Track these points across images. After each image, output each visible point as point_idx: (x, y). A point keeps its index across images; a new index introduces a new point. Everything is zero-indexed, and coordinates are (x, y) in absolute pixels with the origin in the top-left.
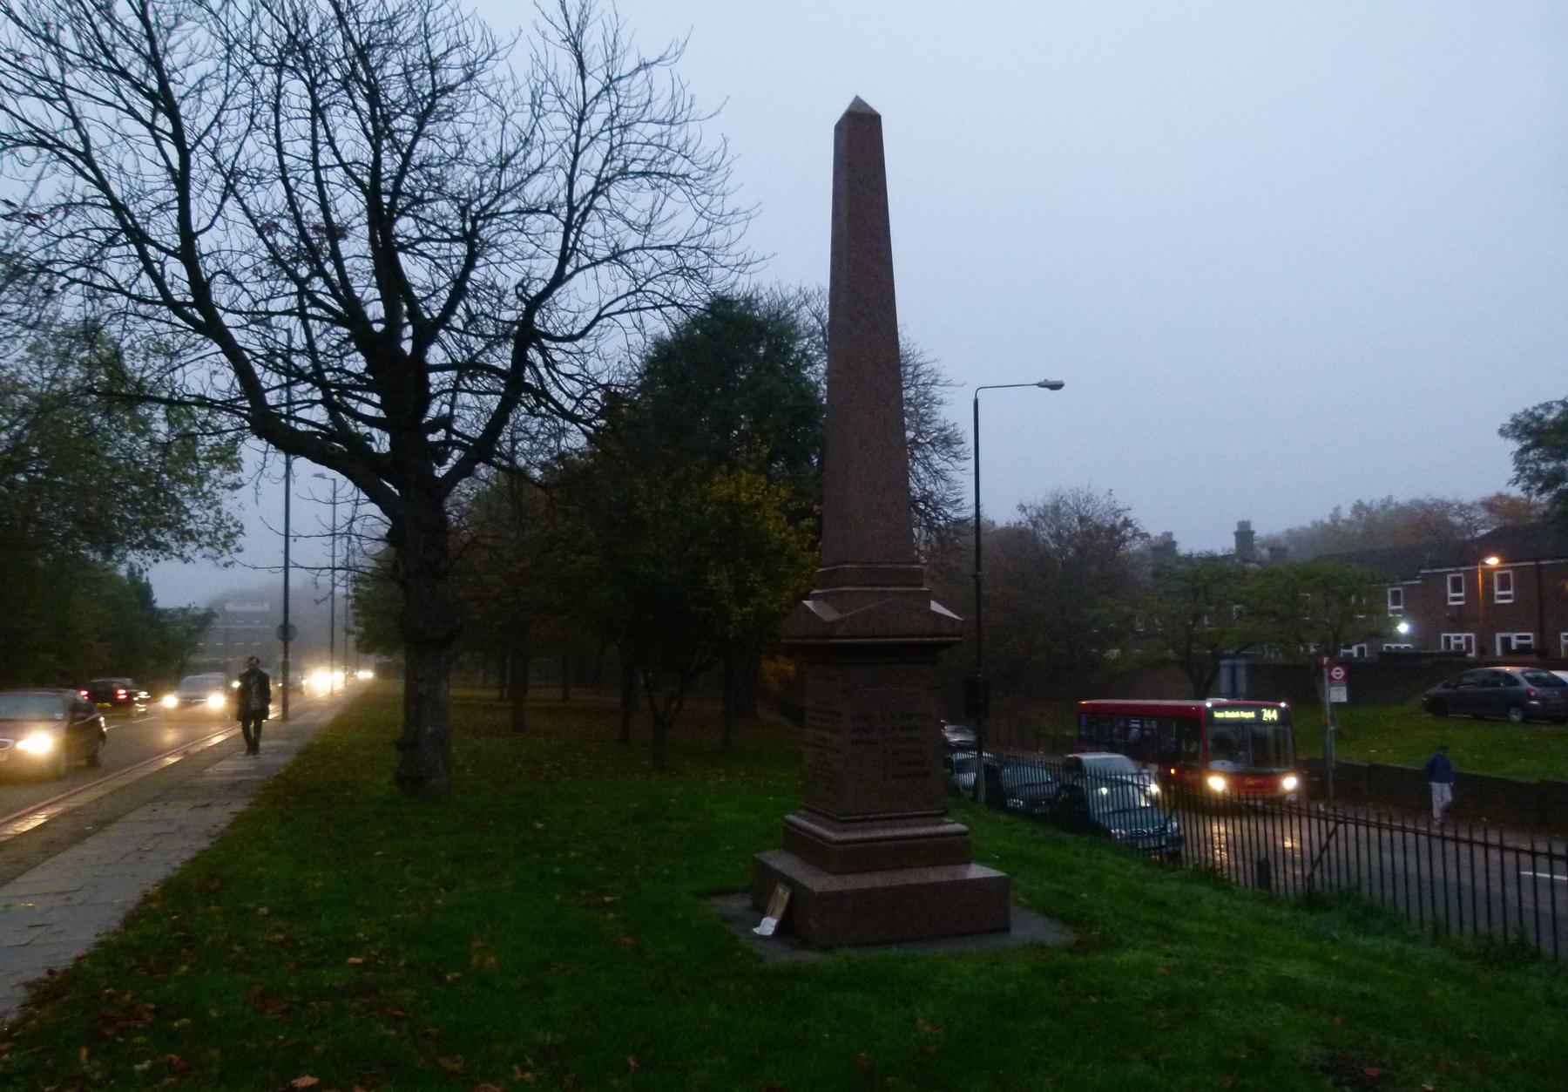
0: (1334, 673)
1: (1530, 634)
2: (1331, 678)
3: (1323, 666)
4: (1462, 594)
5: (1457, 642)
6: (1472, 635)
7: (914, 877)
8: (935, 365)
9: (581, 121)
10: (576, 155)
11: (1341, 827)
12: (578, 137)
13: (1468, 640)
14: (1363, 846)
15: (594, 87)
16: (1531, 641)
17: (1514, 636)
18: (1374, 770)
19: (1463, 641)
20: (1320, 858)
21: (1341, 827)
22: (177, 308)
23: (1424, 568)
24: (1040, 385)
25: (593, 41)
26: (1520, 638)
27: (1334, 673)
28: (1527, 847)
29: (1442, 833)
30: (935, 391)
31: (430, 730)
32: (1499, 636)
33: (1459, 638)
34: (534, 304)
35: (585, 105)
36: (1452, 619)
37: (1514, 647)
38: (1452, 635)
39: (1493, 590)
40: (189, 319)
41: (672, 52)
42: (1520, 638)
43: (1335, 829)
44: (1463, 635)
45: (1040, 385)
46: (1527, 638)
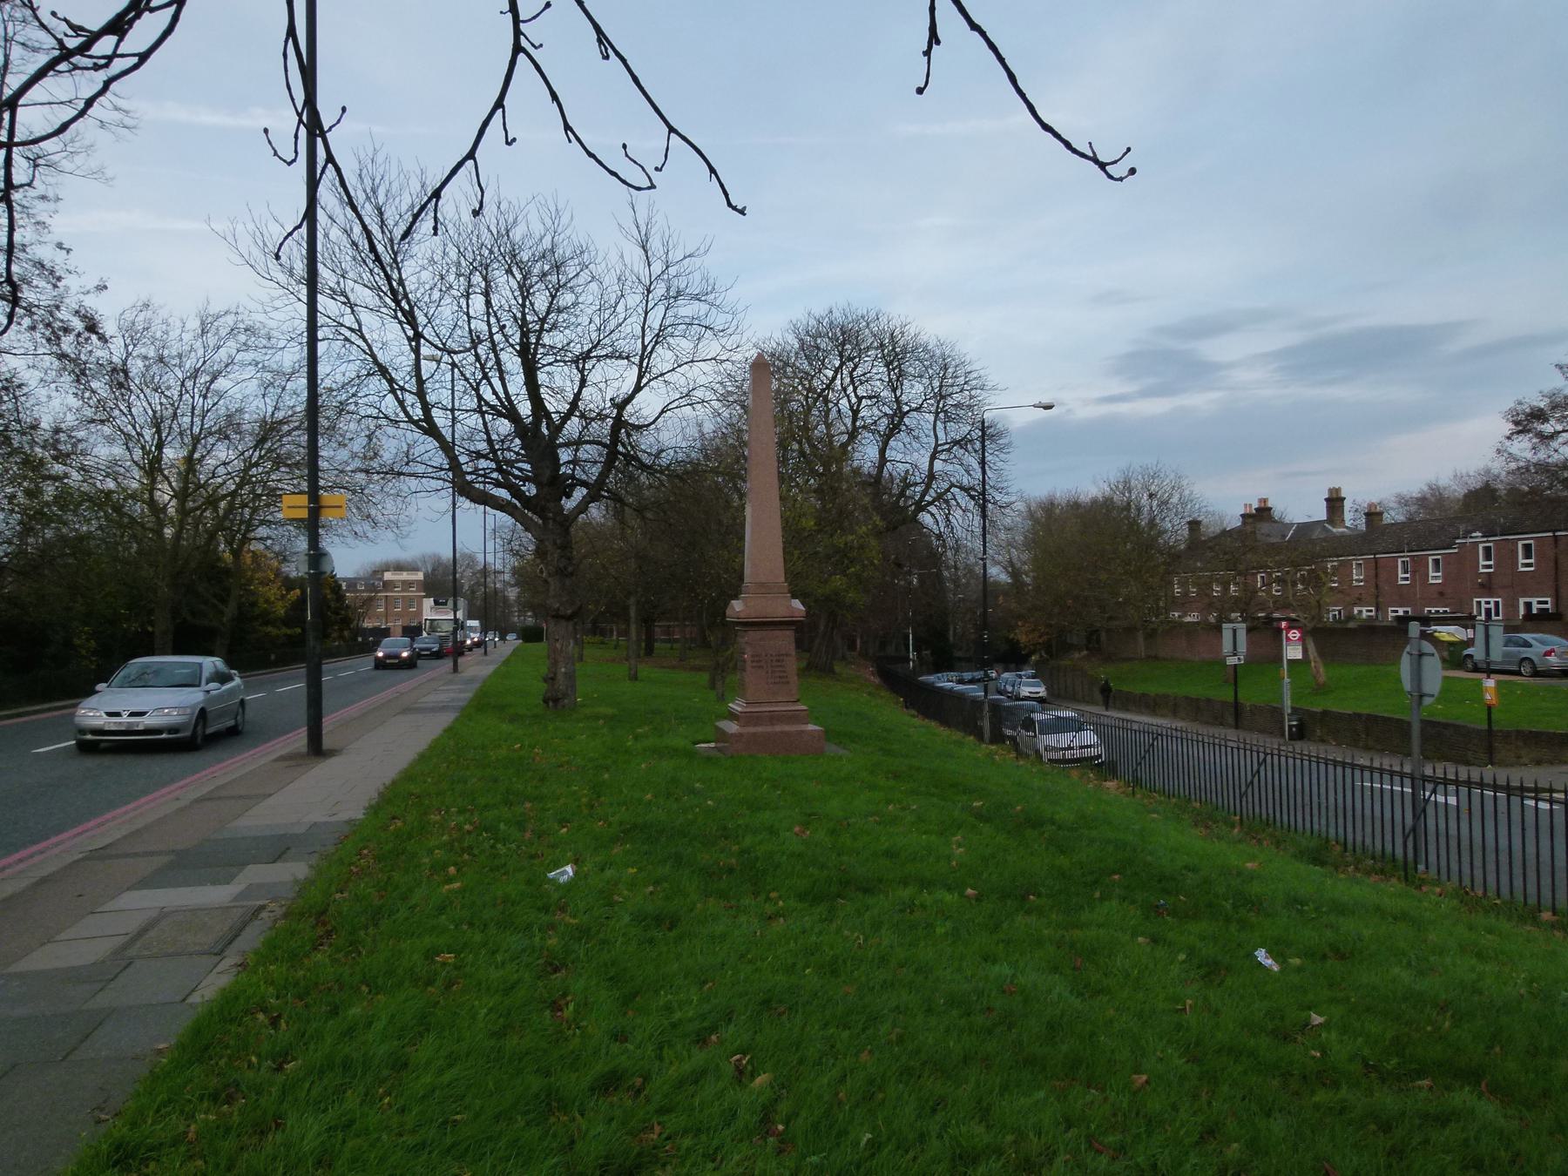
0: (1290, 635)
1: (1549, 599)
2: (1288, 639)
3: (1282, 630)
4: (1491, 563)
5: (1488, 606)
6: (1499, 600)
7: (778, 728)
8: (982, 373)
9: (649, 292)
10: (646, 313)
11: (1269, 757)
12: (647, 302)
13: (1497, 603)
14: (1530, 834)
15: (657, 268)
16: (1548, 606)
17: (1534, 601)
18: (1372, 720)
19: (1492, 606)
20: (1414, 829)
21: (1269, 757)
22: (416, 423)
23: (1458, 538)
24: (1034, 406)
25: (655, 244)
26: (1539, 603)
27: (1290, 635)
28: (1367, 763)
29: (1551, 806)
30: (983, 395)
31: (563, 670)
32: (1522, 601)
33: (1488, 603)
34: (621, 406)
35: (651, 283)
36: (1482, 585)
37: (1535, 611)
38: (1483, 600)
39: (1517, 558)
40: (420, 427)
41: (702, 251)
42: (1539, 603)
43: (1265, 760)
44: (1492, 600)
45: (1034, 406)
46: (1546, 603)
